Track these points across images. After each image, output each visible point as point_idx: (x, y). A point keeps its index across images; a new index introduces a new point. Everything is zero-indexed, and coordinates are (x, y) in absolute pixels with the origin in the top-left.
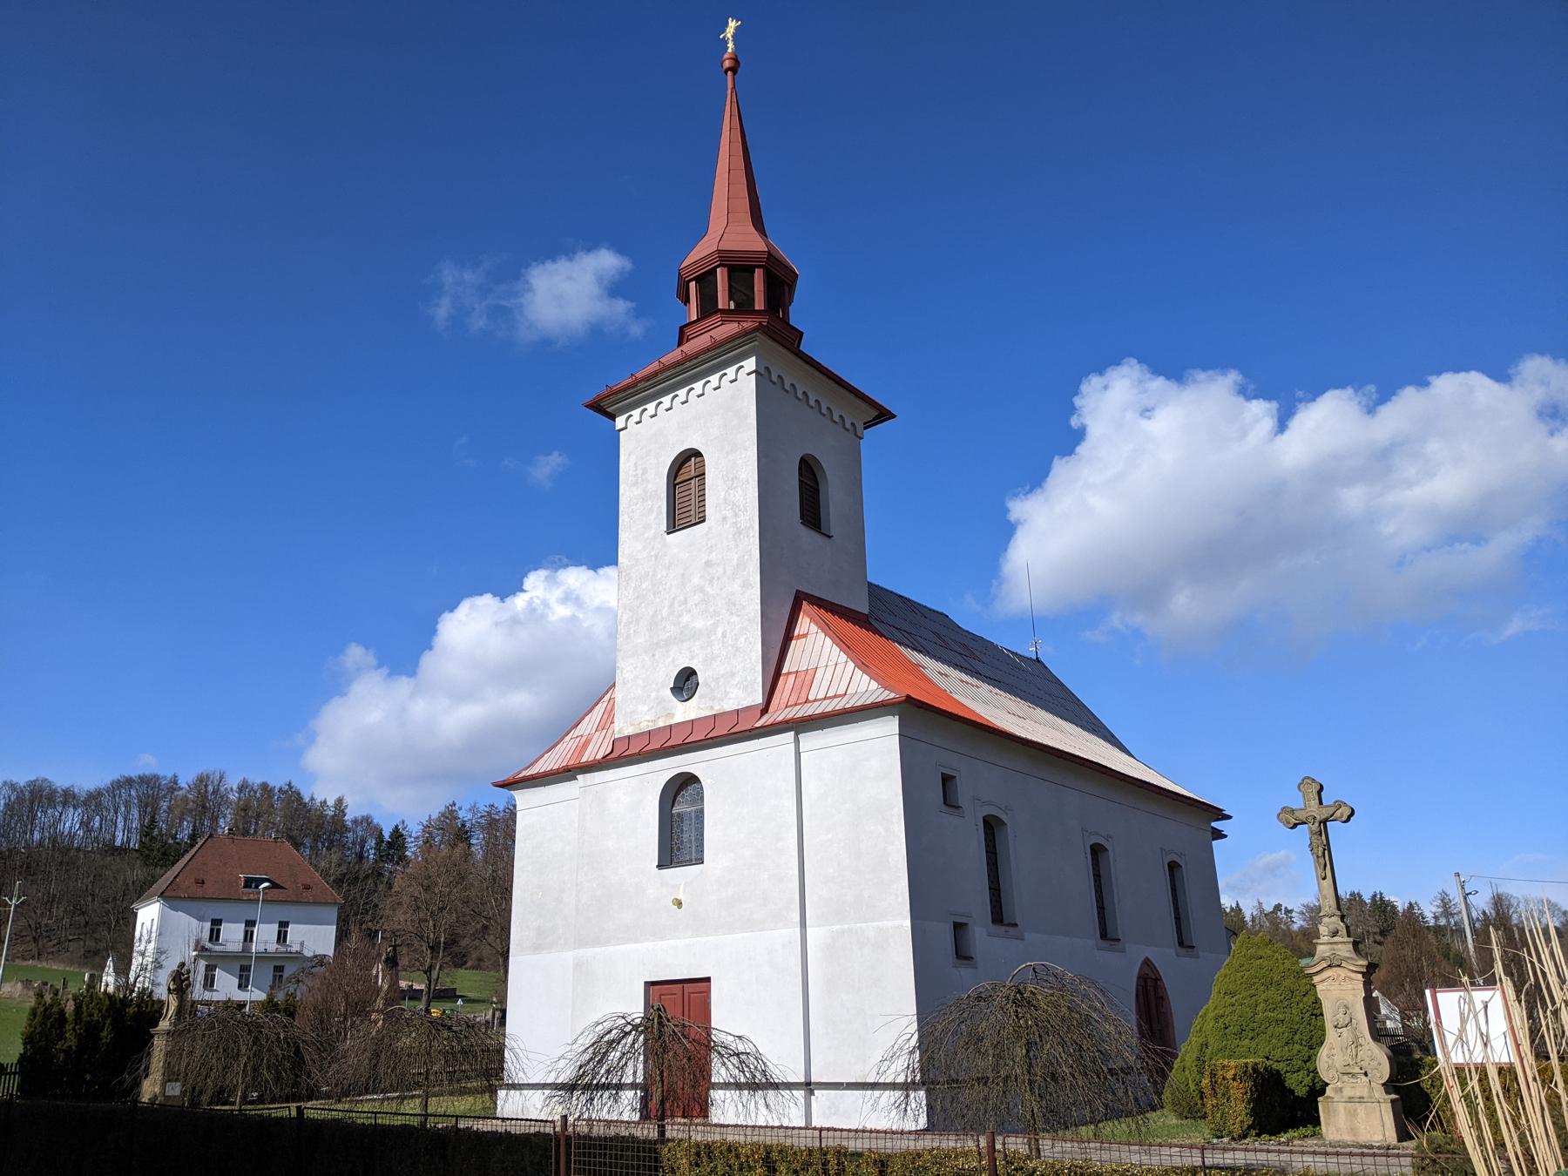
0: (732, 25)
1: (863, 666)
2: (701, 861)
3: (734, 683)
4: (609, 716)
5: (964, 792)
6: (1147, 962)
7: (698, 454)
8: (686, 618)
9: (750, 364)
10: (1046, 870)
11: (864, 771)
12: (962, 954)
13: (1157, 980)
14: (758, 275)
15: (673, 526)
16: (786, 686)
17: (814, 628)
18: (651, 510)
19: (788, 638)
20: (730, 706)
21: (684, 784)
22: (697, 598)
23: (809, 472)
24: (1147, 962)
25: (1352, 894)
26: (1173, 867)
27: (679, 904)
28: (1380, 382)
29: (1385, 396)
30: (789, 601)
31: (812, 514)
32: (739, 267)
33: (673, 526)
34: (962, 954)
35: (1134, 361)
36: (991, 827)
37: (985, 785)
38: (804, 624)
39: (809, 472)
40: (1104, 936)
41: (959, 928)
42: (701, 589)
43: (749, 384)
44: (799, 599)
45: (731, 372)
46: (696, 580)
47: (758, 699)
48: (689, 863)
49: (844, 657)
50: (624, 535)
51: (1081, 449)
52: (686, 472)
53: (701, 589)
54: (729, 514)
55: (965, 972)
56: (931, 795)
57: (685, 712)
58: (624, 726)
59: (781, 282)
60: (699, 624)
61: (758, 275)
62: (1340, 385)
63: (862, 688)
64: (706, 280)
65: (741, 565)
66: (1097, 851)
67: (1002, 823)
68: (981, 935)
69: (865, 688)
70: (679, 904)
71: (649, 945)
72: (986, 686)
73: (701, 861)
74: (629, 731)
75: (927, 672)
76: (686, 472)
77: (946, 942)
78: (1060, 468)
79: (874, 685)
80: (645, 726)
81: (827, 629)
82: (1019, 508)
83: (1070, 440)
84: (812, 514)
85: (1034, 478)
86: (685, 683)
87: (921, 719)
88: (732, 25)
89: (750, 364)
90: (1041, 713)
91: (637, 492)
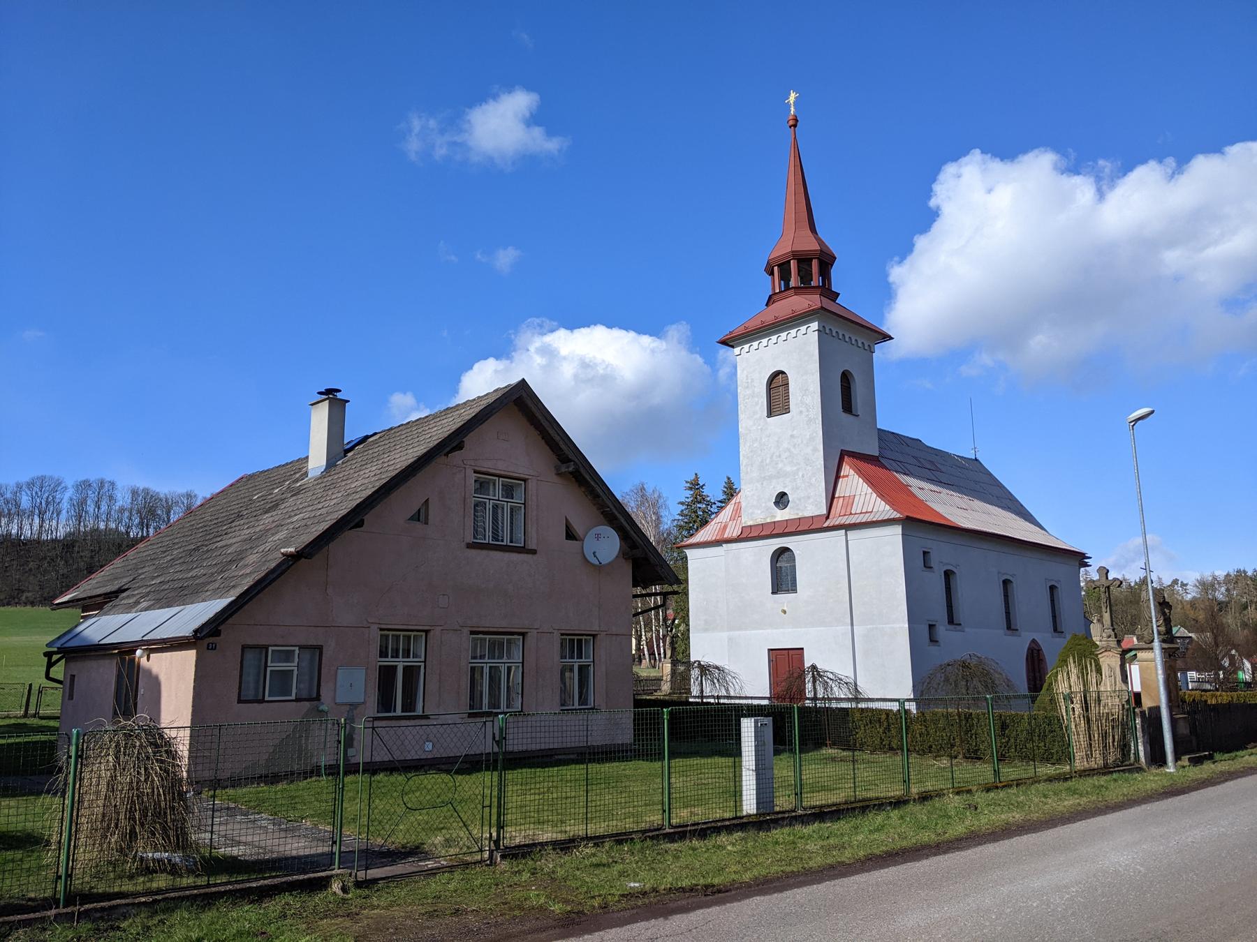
0: (793, 97)
1: (881, 495)
2: (794, 590)
3: (809, 502)
4: (737, 513)
5: (934, 560)
6: (1034, 641)
7: (783, 373)
8: (780, 465)
9: (815, 326)
10: (978, 595)
11: (883, 555)
12: (933, 640)
13: (1039, 650)
14: (815, 263)
15: (770, 414)
16: (838, 505)
17: (852, 472)
18: (757, 404)
19: (838, 477)
20: (808, 514)
21: (782, 552)
22: (787, 454)
23: (846, 378)
24: (1034, 641)
25: (938, 208)
26: (1052, 588)
27: (785, 612)
28: (1179, 155)
29: (1183, 161)
30: (839, 457)
31: (848, 407)
32: (804, 260)
33: (770, 414)
34: (933, 640)
35: (977, 153)
36: (948, 574)
37: (944, 553)
38: (846, 469)
39: (846, 378)
40: (1009, 628)
41: (931, 627)
42: (789, 450)
43: (815, 337)
44: (844, 454)
45: (803, 329)
46: (785, 445)
47: (825, 512)
48: (787, 591)
49: (870, 490)
50: (742, 416)
51: (937, 227)
52: (777, 384)
53: (789, 450)
54: (804, 409)
55: (933, 649)
56: (918, 563)
57: (781, 515)
58: (747, 520)
59: (826, 261)
60: (788, 469)
61: (815, 263)
62: (1144, 161)
63: (881, 509)
64: (784, 267)
65: (812, 439)
66: (1006, 583)
67: (953, 572)
68: (943, 631)
69: (882, 509)
70: (785, 612)
71: (769, 631)
72: (945, 491)
73: (794, 590)
74: (751, 523)
75: (913, 490)
76: (777, 384)
77: (924, 634)
78: (921, 242)
79: (888, 507)
80: (760, 521)
81: (860, 473)
82: (897, 273)
83: (927, 218)
84: (848, 407)
85: (904, 250)
86: (781, 500)
87: (918, 526)
88: (793, 97)
89: (815, 326)
90: (977, 504)
91: (748, 392)
